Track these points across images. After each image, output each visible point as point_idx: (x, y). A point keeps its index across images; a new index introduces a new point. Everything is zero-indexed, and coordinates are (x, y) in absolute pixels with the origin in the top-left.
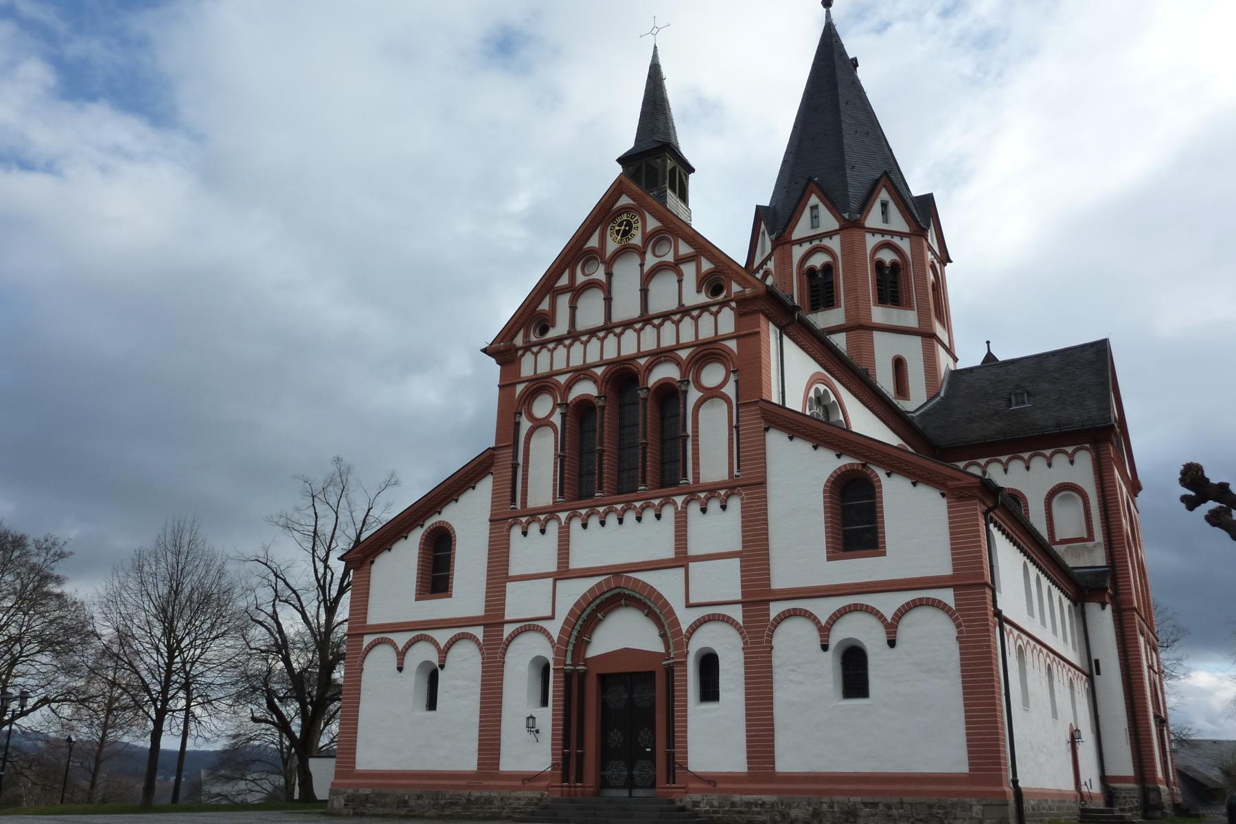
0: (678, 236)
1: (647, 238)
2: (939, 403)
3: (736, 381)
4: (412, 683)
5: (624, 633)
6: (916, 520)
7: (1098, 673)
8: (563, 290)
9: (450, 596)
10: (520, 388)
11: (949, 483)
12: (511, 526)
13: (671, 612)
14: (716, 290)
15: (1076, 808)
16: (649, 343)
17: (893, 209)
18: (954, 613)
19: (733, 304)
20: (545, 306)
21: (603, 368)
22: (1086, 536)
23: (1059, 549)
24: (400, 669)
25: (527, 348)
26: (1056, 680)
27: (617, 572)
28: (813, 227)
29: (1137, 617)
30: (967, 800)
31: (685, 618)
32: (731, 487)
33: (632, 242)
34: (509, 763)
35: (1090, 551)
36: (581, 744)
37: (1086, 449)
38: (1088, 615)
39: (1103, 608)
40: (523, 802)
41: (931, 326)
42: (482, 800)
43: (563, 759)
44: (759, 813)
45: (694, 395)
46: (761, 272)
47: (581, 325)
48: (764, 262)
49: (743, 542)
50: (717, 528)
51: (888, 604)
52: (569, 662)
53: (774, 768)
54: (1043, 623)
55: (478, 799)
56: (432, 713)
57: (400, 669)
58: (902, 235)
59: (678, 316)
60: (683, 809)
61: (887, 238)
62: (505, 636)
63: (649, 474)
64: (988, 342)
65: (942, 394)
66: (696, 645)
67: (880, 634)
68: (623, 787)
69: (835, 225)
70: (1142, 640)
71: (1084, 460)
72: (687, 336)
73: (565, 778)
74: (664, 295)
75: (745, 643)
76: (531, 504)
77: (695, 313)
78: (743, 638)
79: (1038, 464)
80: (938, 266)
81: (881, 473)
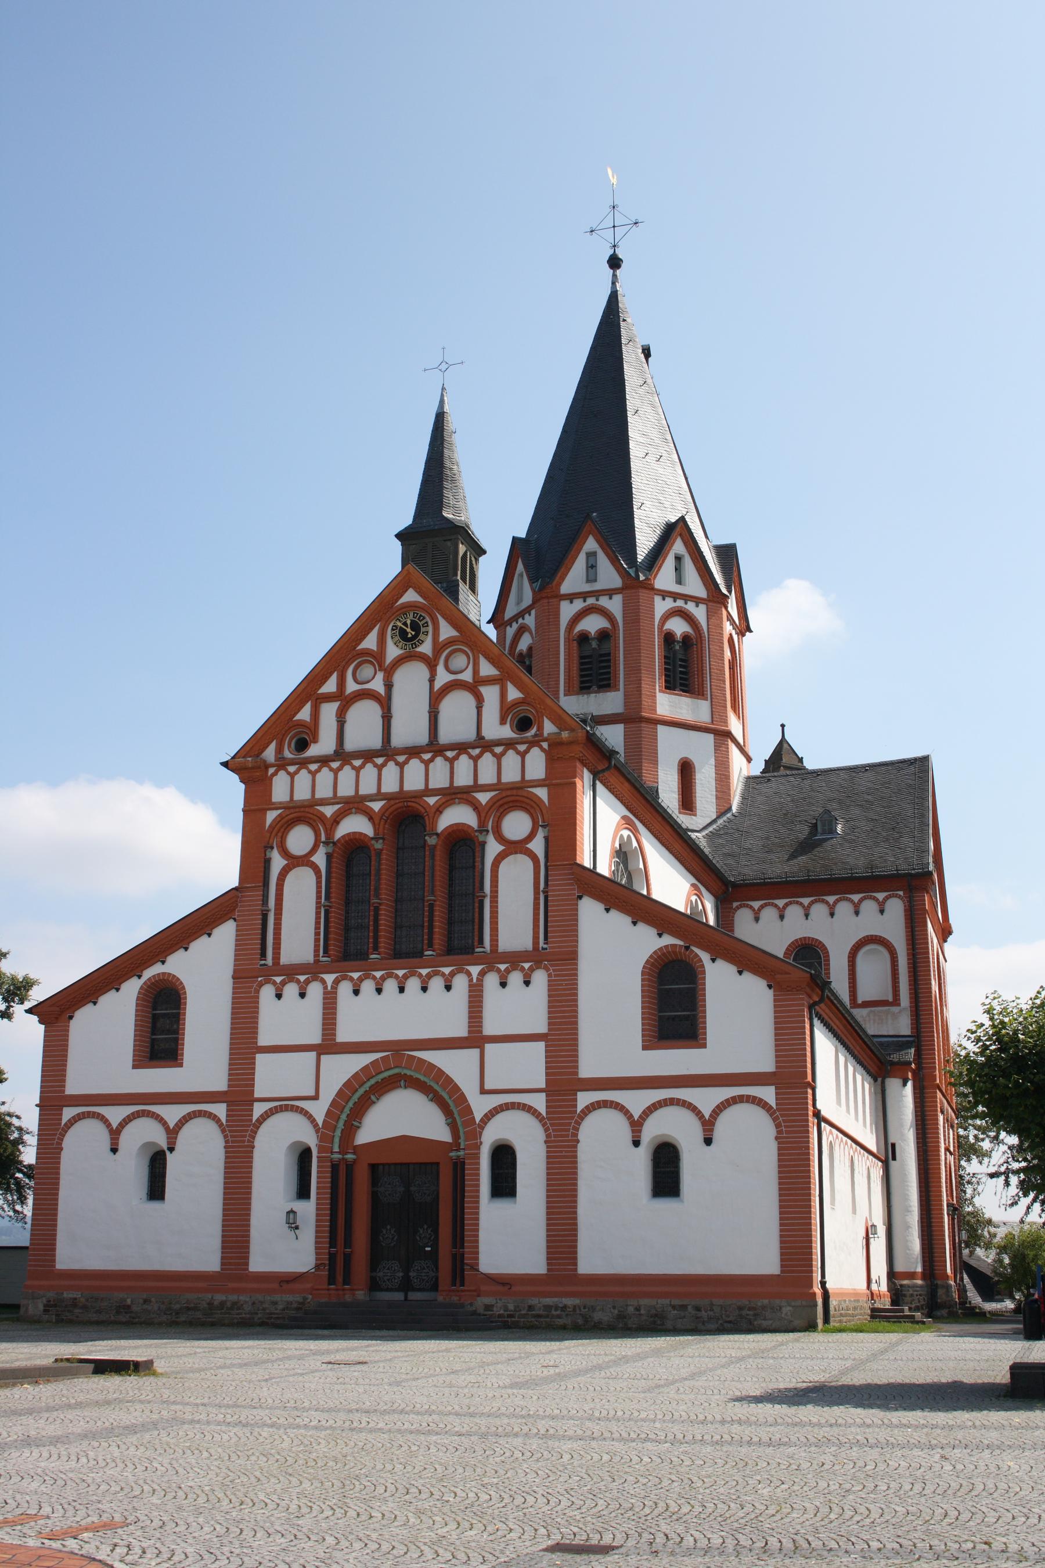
0: (479, 652)
1: (439, 648)
2: (730, 821)
3: (546, 839)
4: (131, 1168)
5: (401, 1118)
6: (738, 1010)
7: (894, 1158)
8: (329, 698)
9: (181, 1065)
10: (271, 816)
11: (778, 976)
12: (261, 985)
13: (462, 1099)
14: (523, 724)
15: (867, 1306)
16: (439, 777)
17: (603, 562)
18: (774, 1112)
19: (545, 745)
20: (304, 714)
21: (382, 803)
22: (891, 999)
23: (859, 1014)
24: (114, 1150)
25: (282, 764)
26: (856, 1172)
27: (398, 1048)
28: (588, 581)
29: (939, 1095)
30: (777, 1302)
31: (480, 1106)
32: (536, 957)
33: (420, 649)
34: (259, 1262)
35: (895, 1017)
36: (348, 1242)
37: (899, 897)
38: (888, 1092)
39: (905, 1085)
40: (280, 1307)
41: (725, 721)
42: (229, 1304)
43: (330, 1259)
44: (559, 1316)
45: (493, 848)
46: (515, 626)
47: (351, 744)
48: (521, 614)
49: (549, 1024)
50: (518, 1005)
51: (707, 1099)
52: (336, 1149)
53: (576, 1270)
54: (857, 1119)
55: (222, 1304)
56: (156, 1205)
57: (114, 1150)
58: (697, 601)
59: (477, 751)
60: (474, 1313)
61: (680, 603)
62: (255, 1117)
63: (436, 936)
64: (783, 726)
65: (734, 809)
66: (490, 1136)
67: (696, 1131)
68: (397, 1290)
69: (617, 582)
70: (941, 1118)
71: (896, 907)
72: (487, 773)
73: (332, 1279)
74: (457, 718)
75: (548, 1136)
76: (284, 960)
77: (498, 750)
78: (546, 1130)
79: (844, 909)
80: (735, 637)
81: (705, 957)
